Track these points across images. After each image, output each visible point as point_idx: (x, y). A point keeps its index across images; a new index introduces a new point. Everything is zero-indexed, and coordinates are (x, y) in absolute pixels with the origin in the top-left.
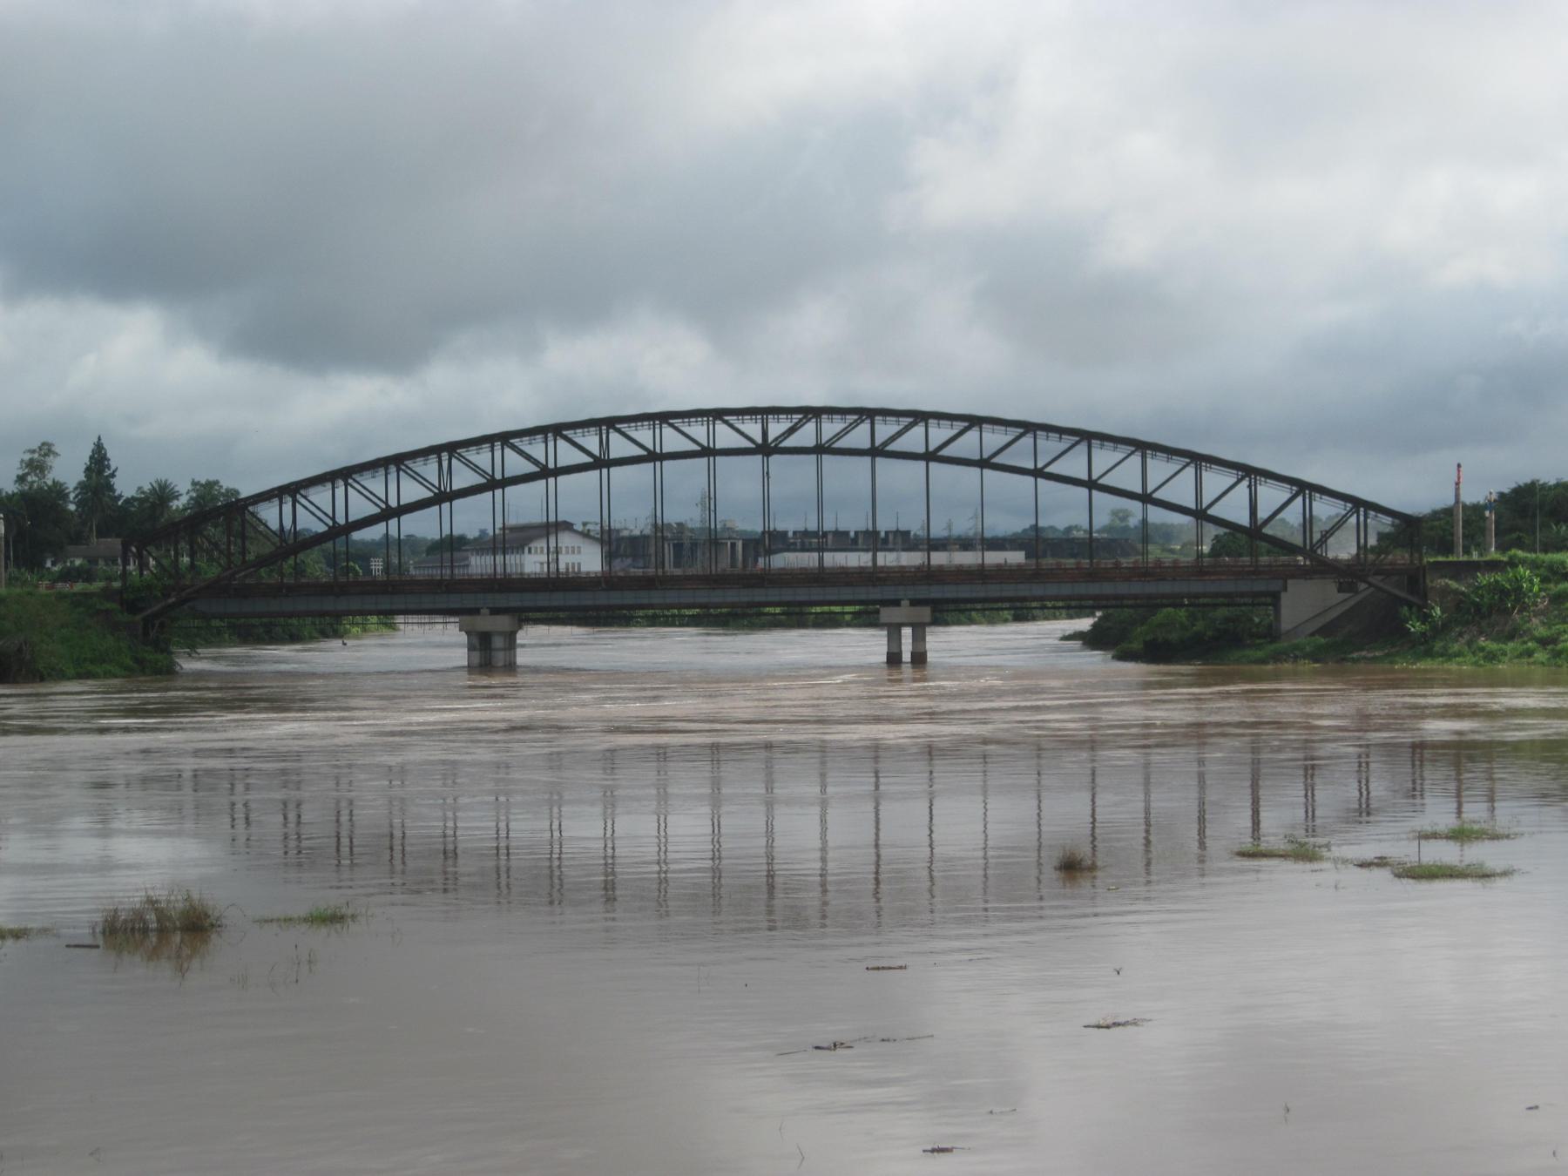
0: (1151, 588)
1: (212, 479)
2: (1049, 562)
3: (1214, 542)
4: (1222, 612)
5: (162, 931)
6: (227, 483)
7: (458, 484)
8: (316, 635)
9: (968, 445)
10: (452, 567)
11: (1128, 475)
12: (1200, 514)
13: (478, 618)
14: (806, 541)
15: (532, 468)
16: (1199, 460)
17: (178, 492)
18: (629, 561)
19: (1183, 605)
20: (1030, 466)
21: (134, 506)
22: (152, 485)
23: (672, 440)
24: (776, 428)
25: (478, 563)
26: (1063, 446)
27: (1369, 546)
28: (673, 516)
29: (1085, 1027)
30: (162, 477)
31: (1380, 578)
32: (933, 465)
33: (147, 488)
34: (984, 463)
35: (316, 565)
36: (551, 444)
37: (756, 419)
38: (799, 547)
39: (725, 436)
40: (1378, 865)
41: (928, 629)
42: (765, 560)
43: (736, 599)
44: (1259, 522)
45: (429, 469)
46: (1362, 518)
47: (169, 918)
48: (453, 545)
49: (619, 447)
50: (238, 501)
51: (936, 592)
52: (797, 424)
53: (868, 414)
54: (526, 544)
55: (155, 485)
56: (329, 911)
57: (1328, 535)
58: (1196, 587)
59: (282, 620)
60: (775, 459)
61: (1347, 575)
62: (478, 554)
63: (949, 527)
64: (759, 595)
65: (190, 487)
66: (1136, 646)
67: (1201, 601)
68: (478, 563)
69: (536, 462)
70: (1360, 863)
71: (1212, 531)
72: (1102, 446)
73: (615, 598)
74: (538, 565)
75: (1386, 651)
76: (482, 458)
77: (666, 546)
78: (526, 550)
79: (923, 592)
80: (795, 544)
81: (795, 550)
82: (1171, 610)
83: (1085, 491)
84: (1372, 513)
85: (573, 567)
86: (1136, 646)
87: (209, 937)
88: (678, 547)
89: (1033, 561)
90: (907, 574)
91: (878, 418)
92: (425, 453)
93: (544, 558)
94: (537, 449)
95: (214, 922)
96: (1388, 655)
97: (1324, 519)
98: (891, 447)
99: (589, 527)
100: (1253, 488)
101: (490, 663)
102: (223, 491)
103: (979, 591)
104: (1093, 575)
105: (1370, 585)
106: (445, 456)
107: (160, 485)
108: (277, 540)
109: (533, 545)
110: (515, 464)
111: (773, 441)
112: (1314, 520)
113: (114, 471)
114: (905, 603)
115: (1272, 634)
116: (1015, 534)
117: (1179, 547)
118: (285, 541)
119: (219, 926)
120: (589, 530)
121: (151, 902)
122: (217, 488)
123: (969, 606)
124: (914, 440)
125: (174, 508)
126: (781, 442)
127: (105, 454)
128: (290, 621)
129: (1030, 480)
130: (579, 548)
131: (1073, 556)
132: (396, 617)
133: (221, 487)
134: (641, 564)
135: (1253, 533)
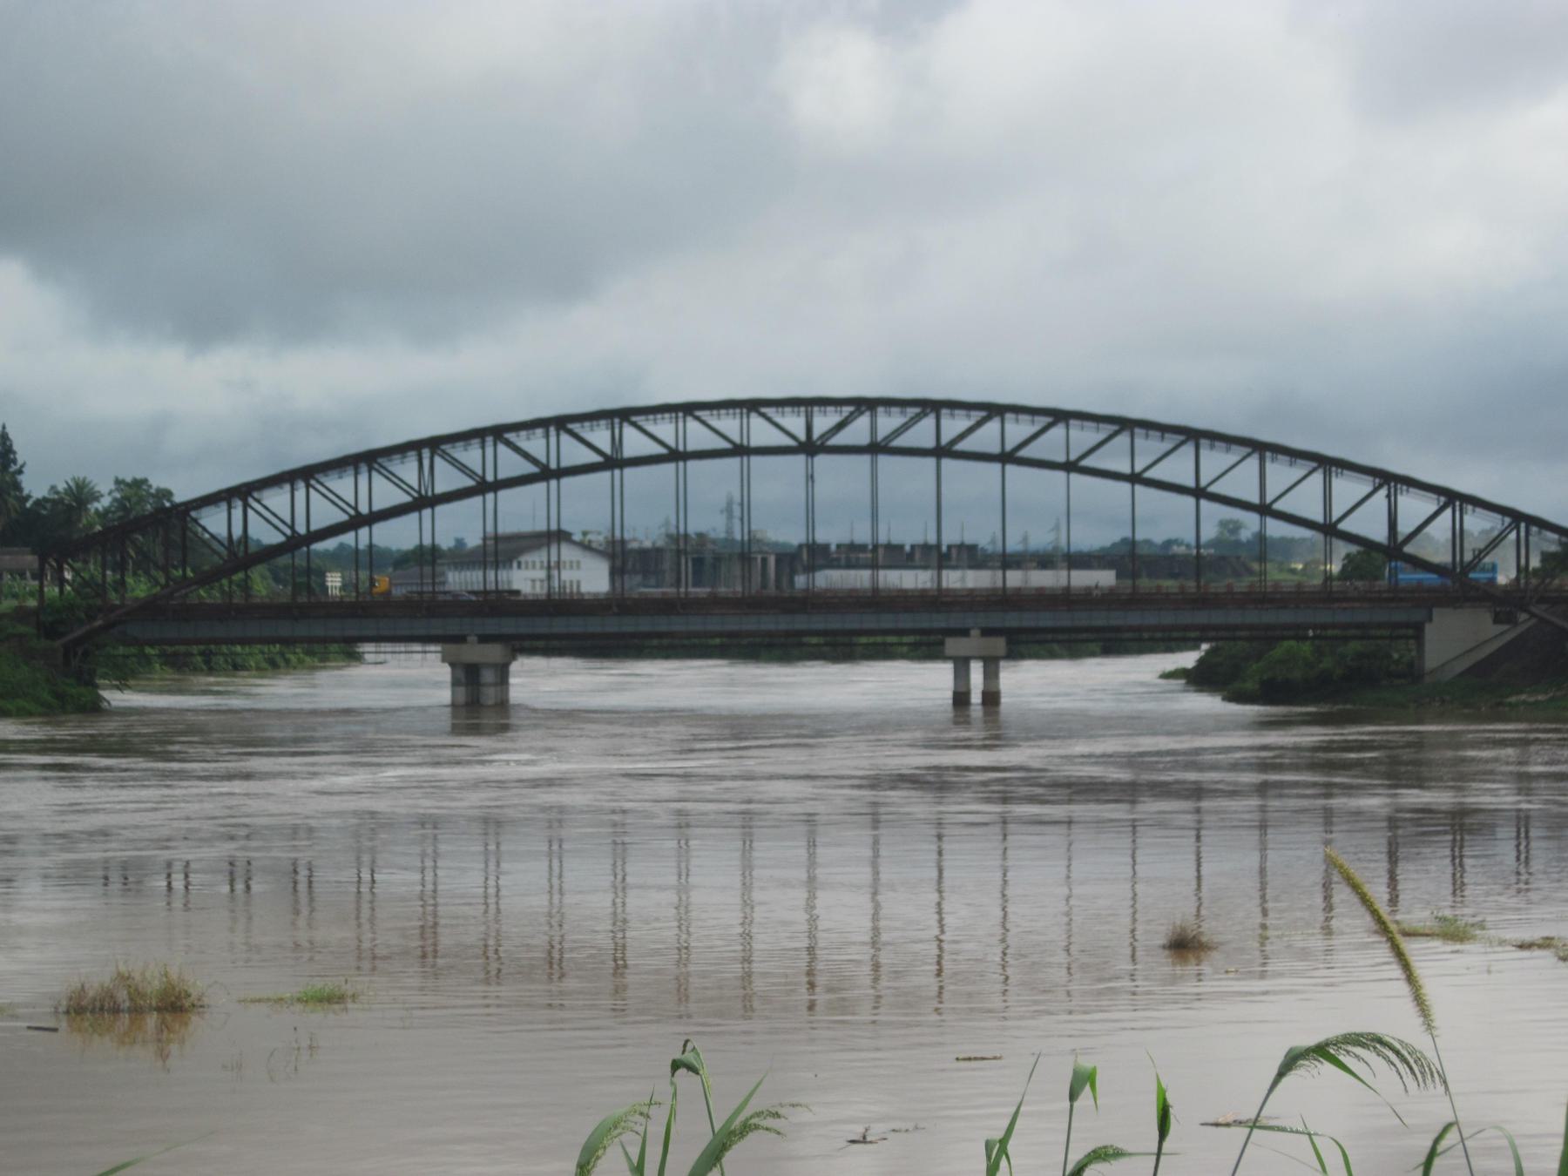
0: (1270, 617)
1: (139, 476)
2: (1145, 583)
3: (1346, 562)
4: (1355, 646)
5: (137, 1011)
6: (157, 482)
7: (440, 488)
8: (264, 665)
9: (1052, 444)
10: (434, 584)
11: (1243, 481)
12: (1329, 529)
14: (853, 556)
15: (530, 469)
16: (1327, 464)
17: (99, 492)
18: (639, 578)
19: (1306, 638)
20: (1126, 469)
21: (45, 508)
22: (67, 483)
23: (697, 436)
24: (823, 422)
25: (457, 580)
26: (1167, 445)
27: (1531, 568)
28: (695, 526)
29: (1202, 1124)
30: (81, 475)
31: (1544, 607)
32: (1010, 468)
33: (61, 487)
34: (1070, 467)
35: (262, 584)
36: (553, 440)
37: (799, 412)
38: (843, 562)
39: (761, 432)
40: (1540, 946)
41: (1002, 664)
42: (808, 578)
43: (772, 627)
44: (1400, 538)
45: (408, 470)
46: (1523, 534)
47: (142, 995)
48: (427, 557)
49: (635, 443)
50: (175, 506)
51: (1012, 620)
52: (847, 418)
53: (932, 407)
54: (515, 557)
55: (72, 484)
56: (327, 990)
57: (1482, 555)
58: (1323, 617)
59: (224, 649)
60: (821, 460)
61: (1504, 603)
62: (456, 568)
63: (1025, 539)
64: (800, 622)
65: (113, 487)
66: (1250, 685)
67: (1330, 632)
68: (457, 580)
69: (534, 461)
70: (1519, 943)
71: (1342, 549)
72: (1212, 447)
73: (628, 625)
74: (529, 583)
75: (1551, 694)
76: (471, 455)
77: (683, 561)
78: (515, 565)
79: (996, 620)
80: (838, 560)
81: (839, 567)
82: (1293, 643)
83: (1191, 501)
84: (1534, 529)
85: (571, 586)
86: (1250, 685)
87: (190, 1018)
88: (698, 562)
89: (1129, 582)
90: (978, 599)
91: (944, 412)
92: (401, 449)
93: (542, 574)
94: (535, 444)
95: (196, 1002)
96: (1552, 699)
97: (1476, 534)
98: (961, 446)
99: (589, 537)
100: (1393, 498)
101: (478, 701)
102: (153, 491)
103: (1064, 619)
104: (1203, 601)
105: (1533, 615)
106: (426, 453)
107: (77, 485)
108: (224, 552)
109: (523, 559)
110: (510, 464)
111: (818, 439)
112: (1465, 536)
113: (22, 466)
114: (975, 633)
115: (1413, 673)
116: (1103, 549)
117: (1300, 567)
118: (235, 555)
119: (202, 1006)
120: (590, 541)
121: (123, 978)
122: (145, 487)
123: (1049, 636)
124: (988, 437)
125: (93, 511)
126: (828, 439)
127: (11, 445)
128: (233, 649)
129: (1125, 487)
130: (578, 562)
131: (1173, 576)
132: (359, 644)
133: (150, 486)
134: (653, 581)
135: (1394, 549)
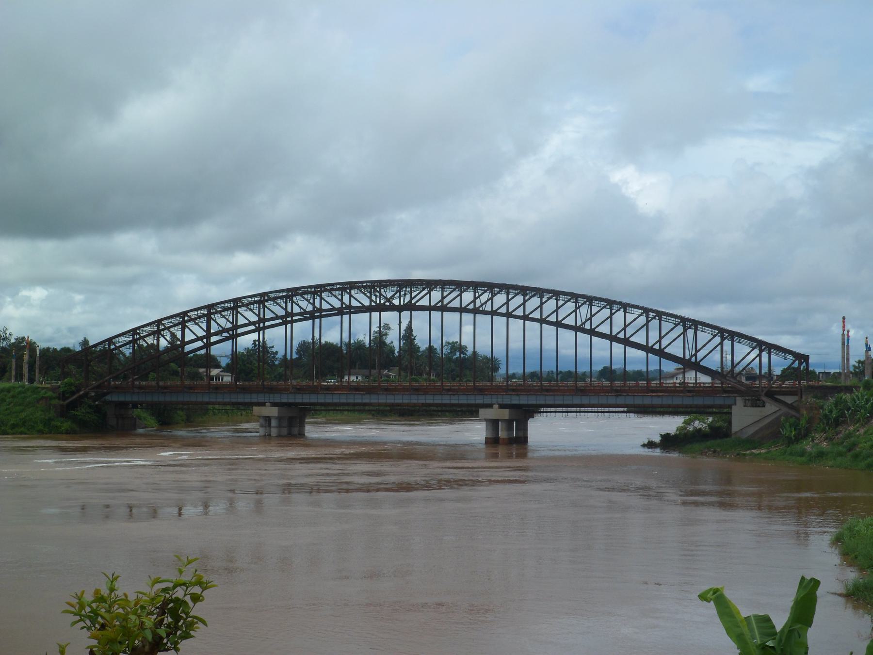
13: (263, 408)
79: (507, 400)
114: (496, 406)
